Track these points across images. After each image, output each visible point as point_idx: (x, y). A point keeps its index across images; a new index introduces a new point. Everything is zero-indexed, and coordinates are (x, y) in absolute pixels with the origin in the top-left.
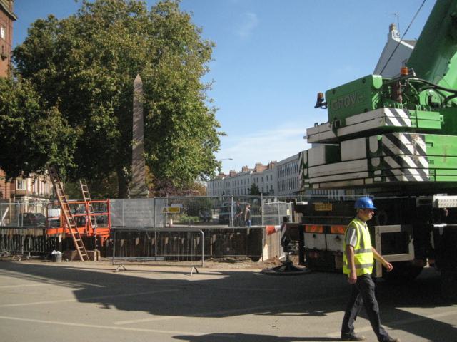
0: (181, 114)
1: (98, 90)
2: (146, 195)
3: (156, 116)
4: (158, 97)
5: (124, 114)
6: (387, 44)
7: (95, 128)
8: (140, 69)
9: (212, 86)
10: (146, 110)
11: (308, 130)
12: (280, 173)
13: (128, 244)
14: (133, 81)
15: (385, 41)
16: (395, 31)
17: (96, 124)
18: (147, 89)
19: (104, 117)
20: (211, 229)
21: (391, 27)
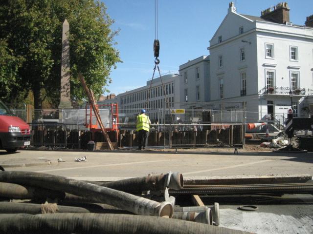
0: (100, 50)
1: (37, 29)
2: (193, 146)
3: (81, 51)
4: (81, 37)
5: (56, 49)
6: (227, 16)
7: (33, 57)
8: (67, 16)
9: (118, 33)
10: (72, 48)
11: (180, 66)
12: (122, 102)
13: (87, 92)
14: (62, 25)
15: (226, 13)
16: (233, 8)
17: (34, 53)
18: (73, 30)
19: (40, 49)
20: (233, 197)
21: (230, 6)
